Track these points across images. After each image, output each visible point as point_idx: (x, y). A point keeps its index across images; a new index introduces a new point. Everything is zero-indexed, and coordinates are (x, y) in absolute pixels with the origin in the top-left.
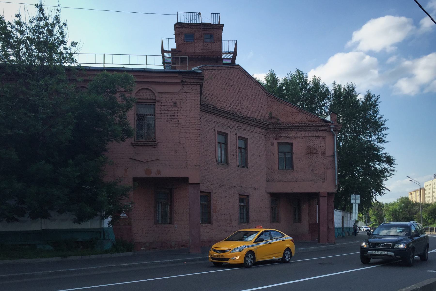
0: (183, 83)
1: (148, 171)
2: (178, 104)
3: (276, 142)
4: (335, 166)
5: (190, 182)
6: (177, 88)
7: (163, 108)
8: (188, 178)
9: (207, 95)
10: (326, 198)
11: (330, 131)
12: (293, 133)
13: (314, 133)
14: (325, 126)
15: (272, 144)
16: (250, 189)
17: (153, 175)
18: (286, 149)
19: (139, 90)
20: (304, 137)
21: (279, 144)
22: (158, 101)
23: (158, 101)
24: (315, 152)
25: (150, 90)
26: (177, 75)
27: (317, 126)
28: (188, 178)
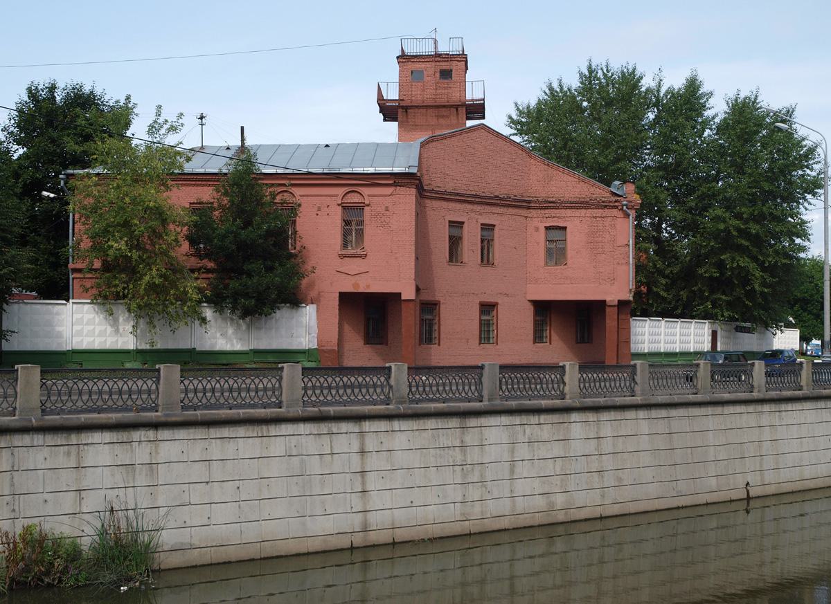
0: (395, 185)
1: (356, 285)
2: (390, 208)
3: (542, 226)
4: (629, 261)
5: (403, 298)
6: (389, 190)
7: (373, 213)
8: (400, 293)
9: (434, 175)
10: (616, 308)
11: (622, 209)
12: (569, 213)
13: (599, 212)
14: (616, 202)
15: (537, 229)
16: (499, 295)
17: (361, 290)
18: (555, 235)
19: (345, 194)
20: (584, 219)
21: (547, 228)
22: (368, 205)
23: (368, 205)
24: (600, 239)
25: (358, 192)
26: (389, 176)
27: (603, 202)
28: (400, 293)
